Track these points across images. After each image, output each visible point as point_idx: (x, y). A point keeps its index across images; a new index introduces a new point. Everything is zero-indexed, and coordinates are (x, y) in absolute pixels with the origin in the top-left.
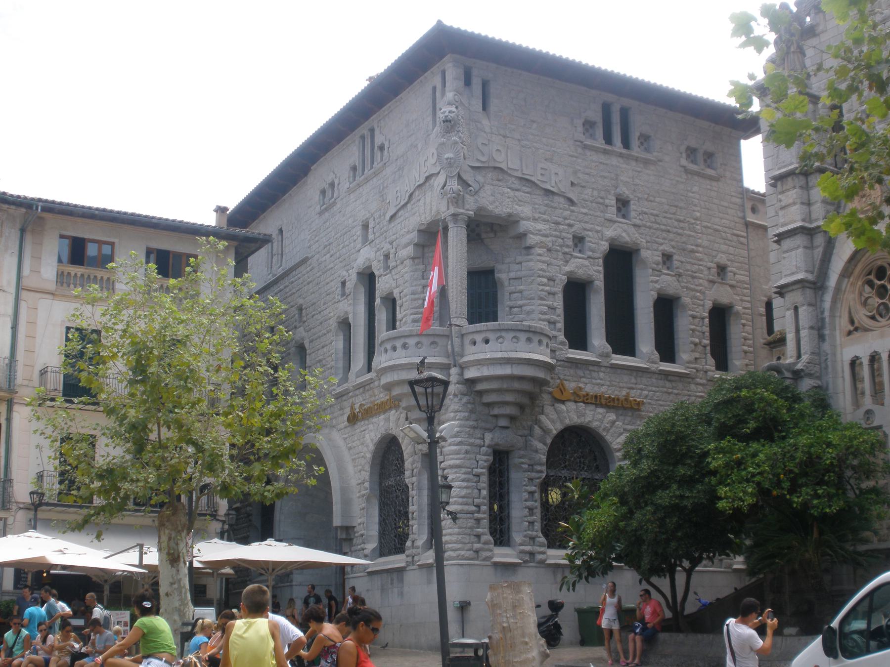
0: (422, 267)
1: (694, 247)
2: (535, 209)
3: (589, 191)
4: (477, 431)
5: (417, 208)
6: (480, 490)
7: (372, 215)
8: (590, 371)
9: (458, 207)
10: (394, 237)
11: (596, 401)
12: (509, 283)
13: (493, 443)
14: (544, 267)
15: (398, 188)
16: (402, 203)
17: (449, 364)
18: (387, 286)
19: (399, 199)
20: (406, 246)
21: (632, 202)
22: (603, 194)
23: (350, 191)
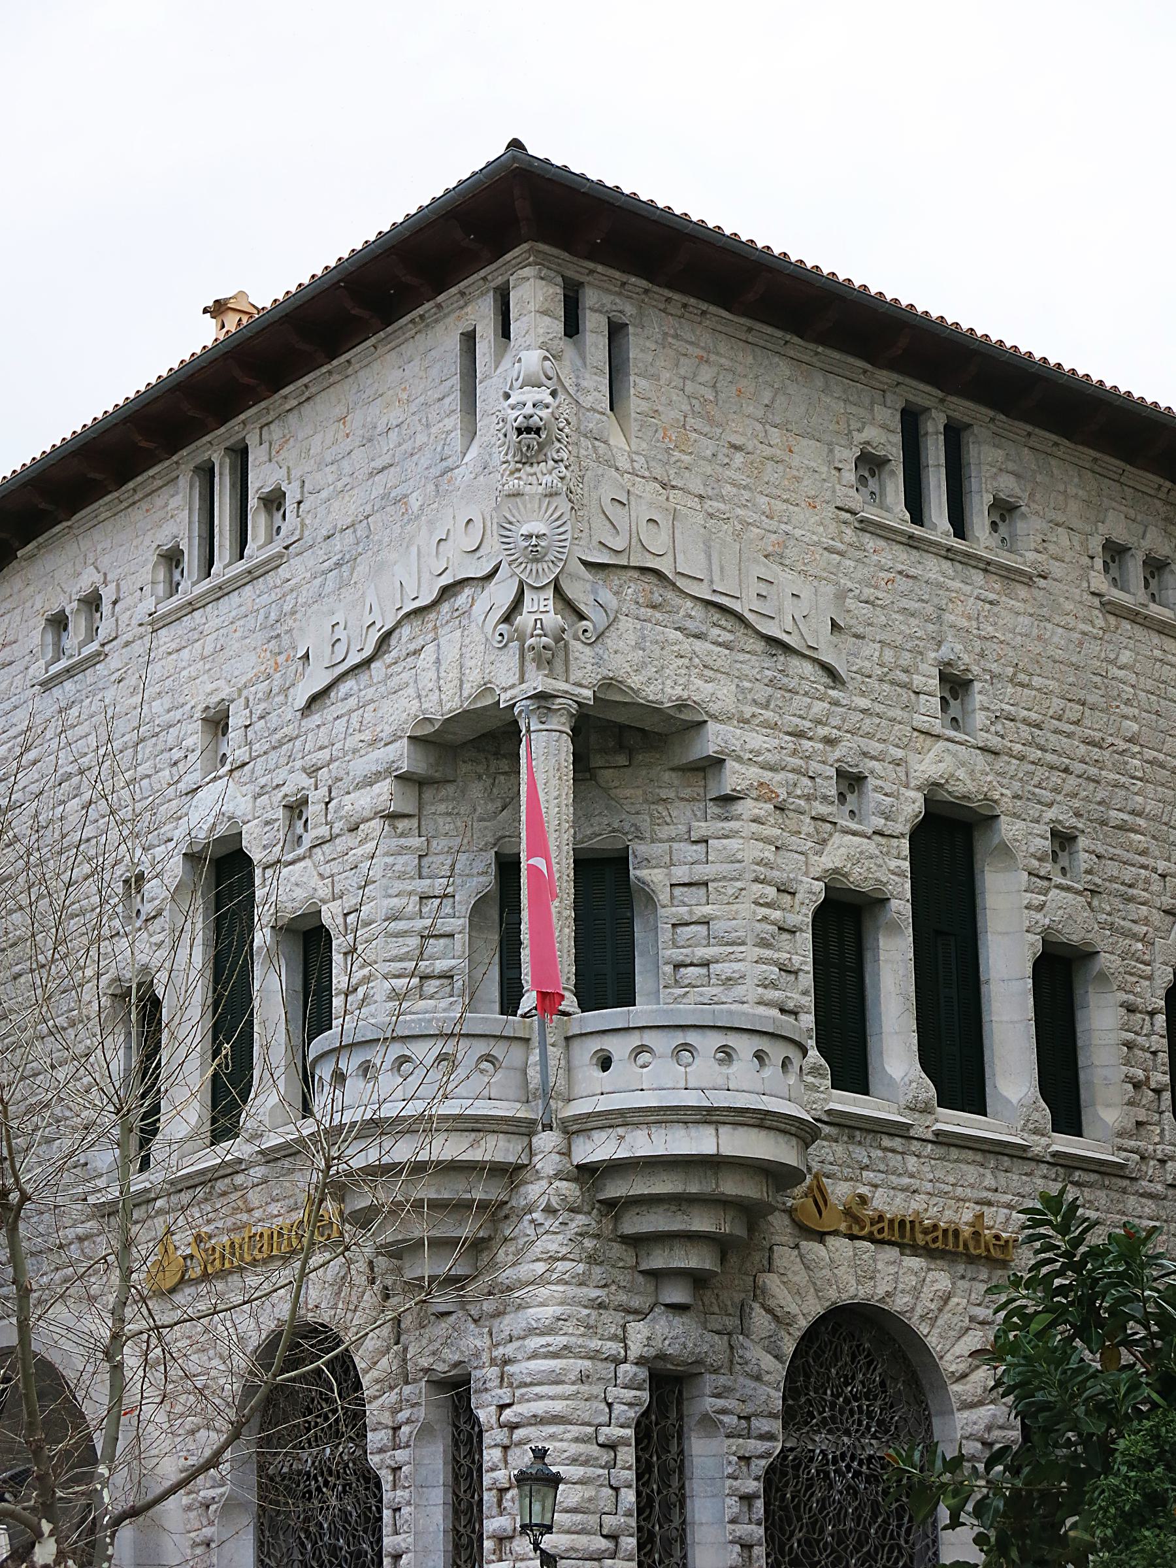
0: (416, 842)
1: (1126, 817)
2: (743, 691)
3: (870, 649)
4: (607, 1316)
5: (405, 676)
6: (616, 1489)
7: (240, 690)
8: (885, 1149)
9: (551, 675)
10: (324, 755)
11: (902, 1236)
12: (672, 897)
13: (652, 1352)
14: (767, 854)
15: (339, 617)
16: (354, 659)
17: (533, 1122)
18: (300, 893)
19: (341, 649)
20: (369, 781)
21: (977, 686)
22: (906, 659)
23: (157, 623)
